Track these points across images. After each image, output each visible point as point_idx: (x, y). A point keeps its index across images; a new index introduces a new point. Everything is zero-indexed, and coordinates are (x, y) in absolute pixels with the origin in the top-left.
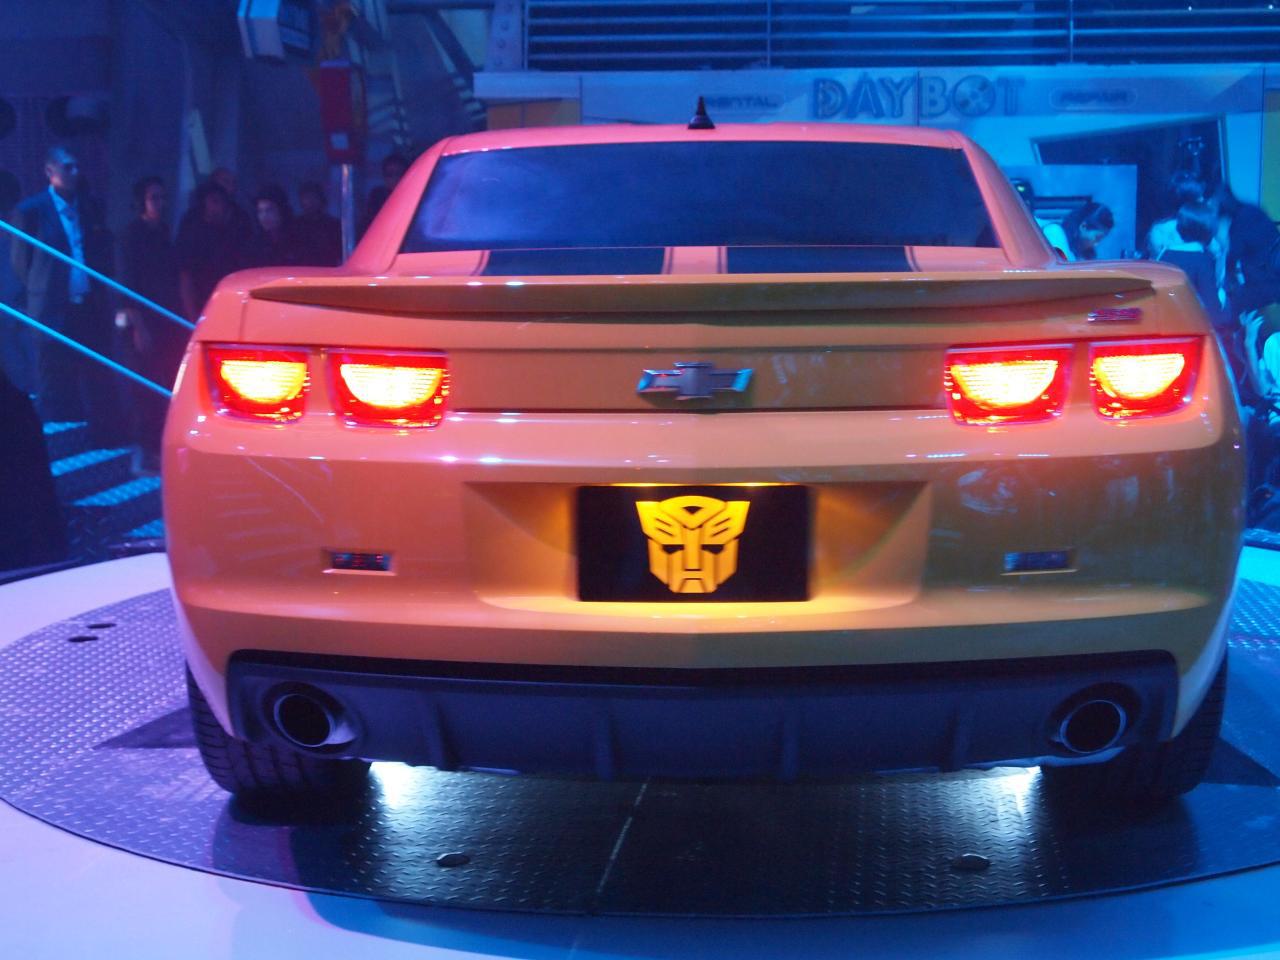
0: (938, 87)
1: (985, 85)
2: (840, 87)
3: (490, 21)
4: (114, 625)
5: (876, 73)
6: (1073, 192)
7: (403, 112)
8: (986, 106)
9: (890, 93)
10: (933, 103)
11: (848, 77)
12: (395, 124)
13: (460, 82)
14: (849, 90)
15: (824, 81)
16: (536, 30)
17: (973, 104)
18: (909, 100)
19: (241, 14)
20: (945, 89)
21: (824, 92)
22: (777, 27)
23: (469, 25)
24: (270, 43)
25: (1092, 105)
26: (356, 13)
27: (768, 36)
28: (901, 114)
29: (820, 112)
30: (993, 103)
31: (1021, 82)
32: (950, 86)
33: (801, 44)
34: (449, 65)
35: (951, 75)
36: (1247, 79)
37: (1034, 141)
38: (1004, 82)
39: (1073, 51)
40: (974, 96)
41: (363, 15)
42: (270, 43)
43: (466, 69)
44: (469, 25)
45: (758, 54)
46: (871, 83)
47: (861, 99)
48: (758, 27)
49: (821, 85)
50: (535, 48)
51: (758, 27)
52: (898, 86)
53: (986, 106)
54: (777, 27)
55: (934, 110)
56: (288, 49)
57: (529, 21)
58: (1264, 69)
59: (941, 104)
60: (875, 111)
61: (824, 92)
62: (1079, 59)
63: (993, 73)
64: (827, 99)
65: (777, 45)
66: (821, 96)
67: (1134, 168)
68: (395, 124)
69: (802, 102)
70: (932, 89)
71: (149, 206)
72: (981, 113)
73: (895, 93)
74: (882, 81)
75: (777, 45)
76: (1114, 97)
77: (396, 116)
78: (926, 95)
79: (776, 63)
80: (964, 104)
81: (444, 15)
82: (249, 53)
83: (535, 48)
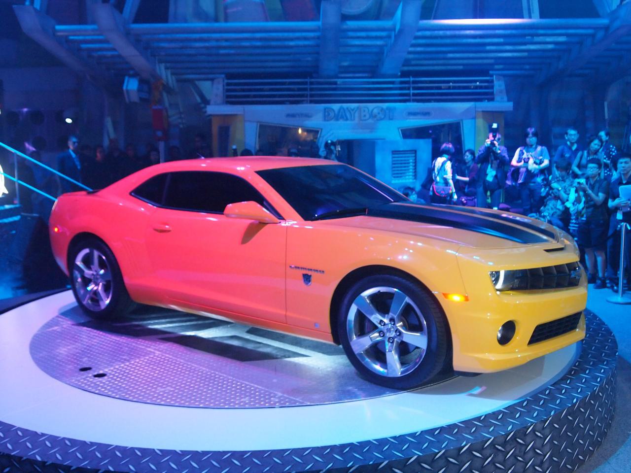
0: (366, 110)
1: (382, 109)
2: (333, 110)
3: (213, 84)
4: (95, 376)
5: (345, 105)
6: (411, 149)
7: (183, 116)
8: (383, 117)
9: (350, 113)
10: (365, 116)
11: (336, 107)
12: (180, 121)
13: (203, 105)
14: (336, 112)
15: (328, 108)
16: (228, 90)
17: (378, 116)
18: (357, 115)
19: (125, 88)
20: (369, 110)
21: (328, 112)
22: (311, 89)
23: (206, 86)
24: (135, 98)
25: (419, 117)
26: (165, 83)
27: (308, 86)
28: (354, 119)
29: (327, 119)
30: (385, 116)
31: (395, 108)
32: (370, 110)
33: (321, 95)
34: (199, 100)
35: (371, 106)
36: (471, 107)
37: (398, 129)
38: (389, 109)
39: (412, 98)
40: (379, 113)
41: (167, 84)
42: (135, 98)
43: (206, 102)
44: (206, 86)
45: (305, 99)
46: (344, 109)
47: (340, 114)
48: (305, 89)
49: (327, 110)
50: (228, 97)
51: (305, 89)
52: (353, 110)
53: (383, 117)
54: (311, 89)
55: (365, 118)
56: (141, 99)
57: (226, 87)
58: (475, 105)
59: (368, 116)
60: (345, 118)
61: (328, 112)
62: (415, 101)
63: (385, 105)
64: (329, 114)
65: (312, 96)
66: (326, 114)
67: (430, 140)
68: (180, 121)
69: (321, 115)
70: (364, 111)
71: (98, 155)
72: (381, 119)
73: (352, 112)
74: (347, 108)
75: (312, 96)
76: (426, 114)
77: (180, 118)
78: (363, 114)
79: (311, 102)
80: (375, 116)
81: (197, 82)
82: (127, 100)
83: (228, 97)
